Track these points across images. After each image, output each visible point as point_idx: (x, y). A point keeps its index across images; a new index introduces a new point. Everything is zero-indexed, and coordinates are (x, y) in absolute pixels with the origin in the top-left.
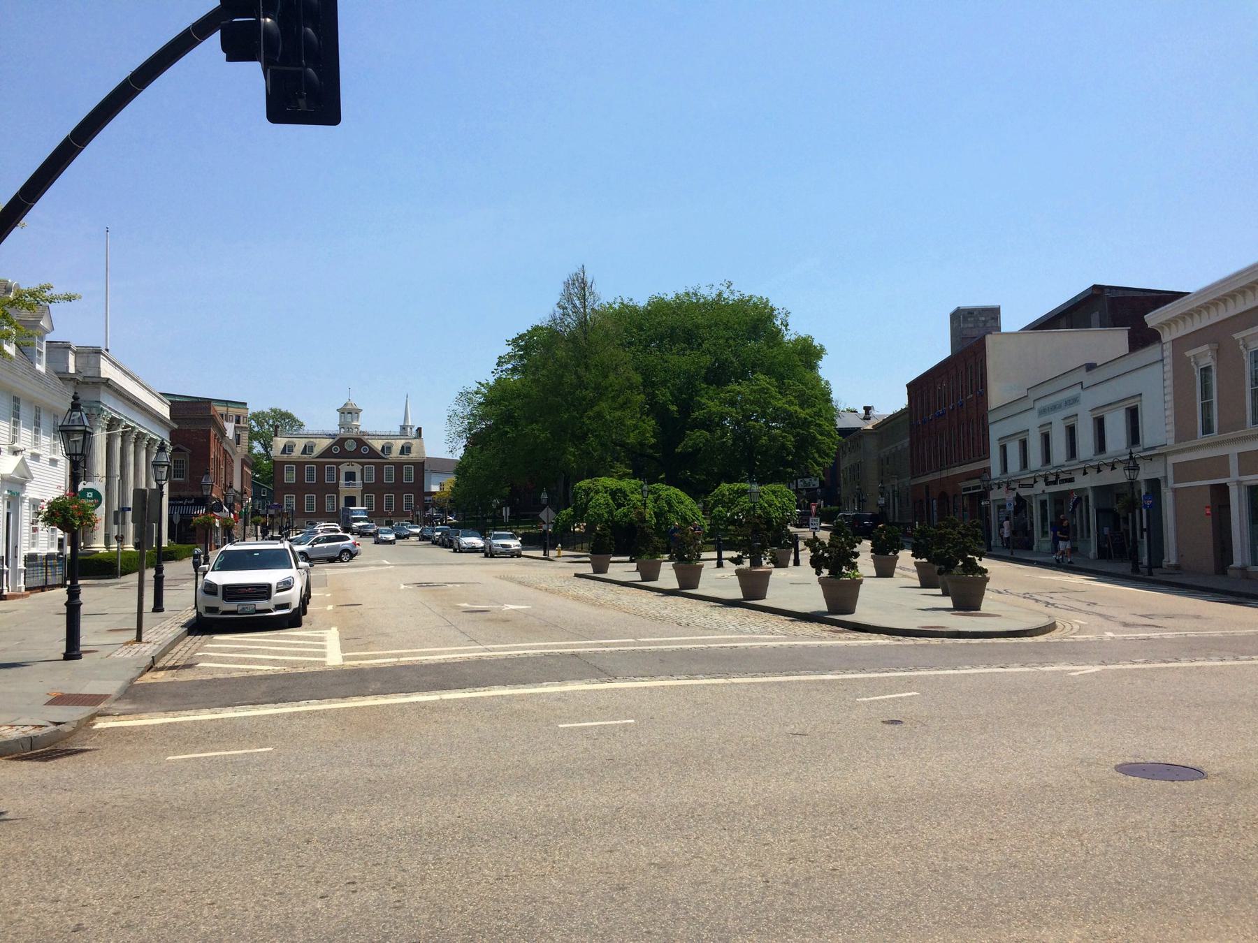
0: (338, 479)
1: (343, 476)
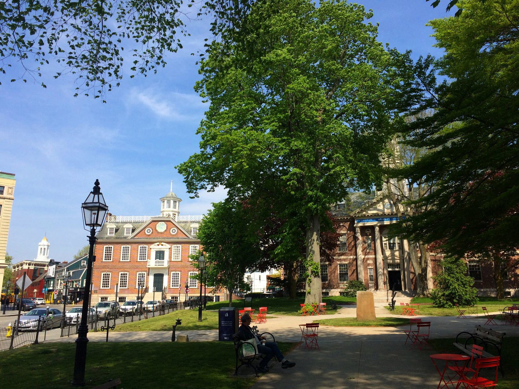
0: (149, 257)
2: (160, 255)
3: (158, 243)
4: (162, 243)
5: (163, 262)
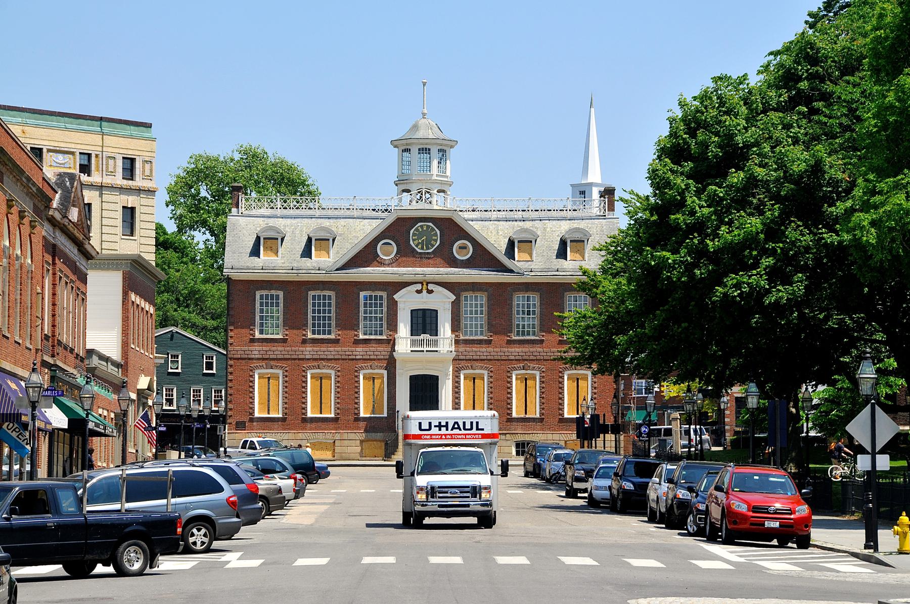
3: (419, 287)
4: (431, 287)
5: (436, 343)
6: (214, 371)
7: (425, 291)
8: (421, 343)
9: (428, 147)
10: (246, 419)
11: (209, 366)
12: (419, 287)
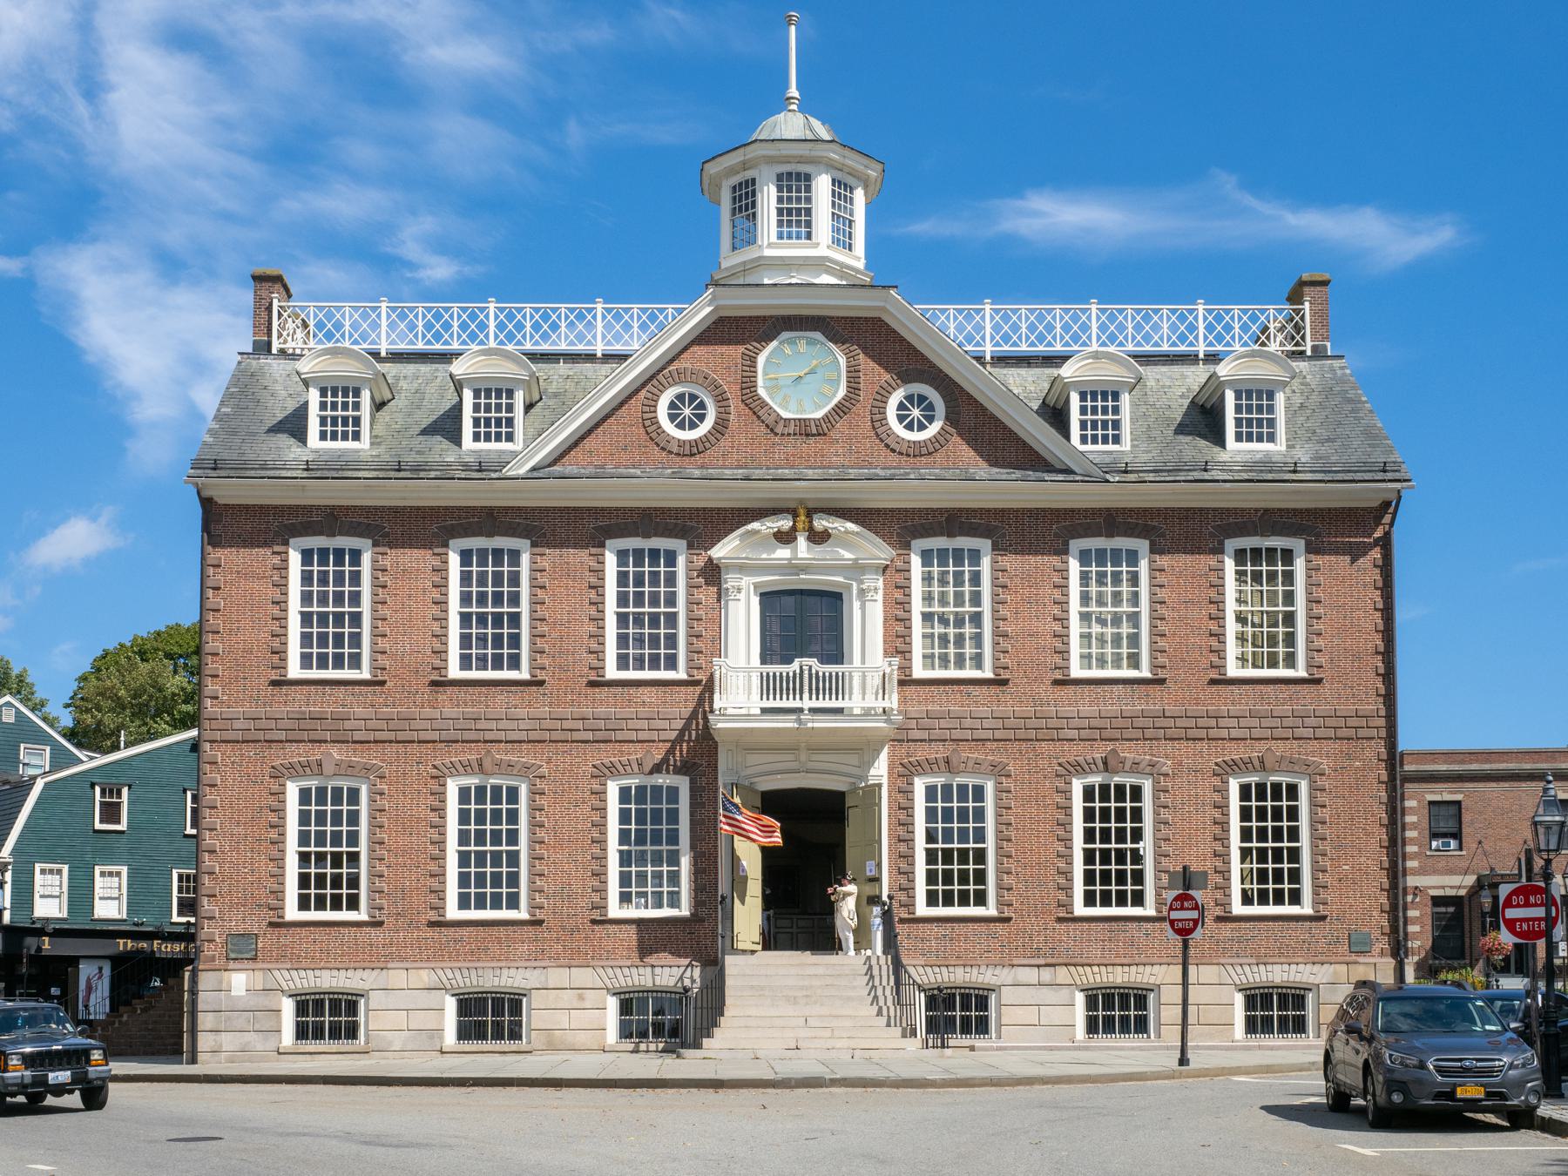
1: (743, 620)
2: (805, 624)
3: (785, 523)
4: (820, 523)
5: (837, 686)
6: (123, 827)
7: (802, 541)
8: (792, 686)
9: (803, 168)
10: (255, 924)
11: (111, 813)
12: (785, 523)
